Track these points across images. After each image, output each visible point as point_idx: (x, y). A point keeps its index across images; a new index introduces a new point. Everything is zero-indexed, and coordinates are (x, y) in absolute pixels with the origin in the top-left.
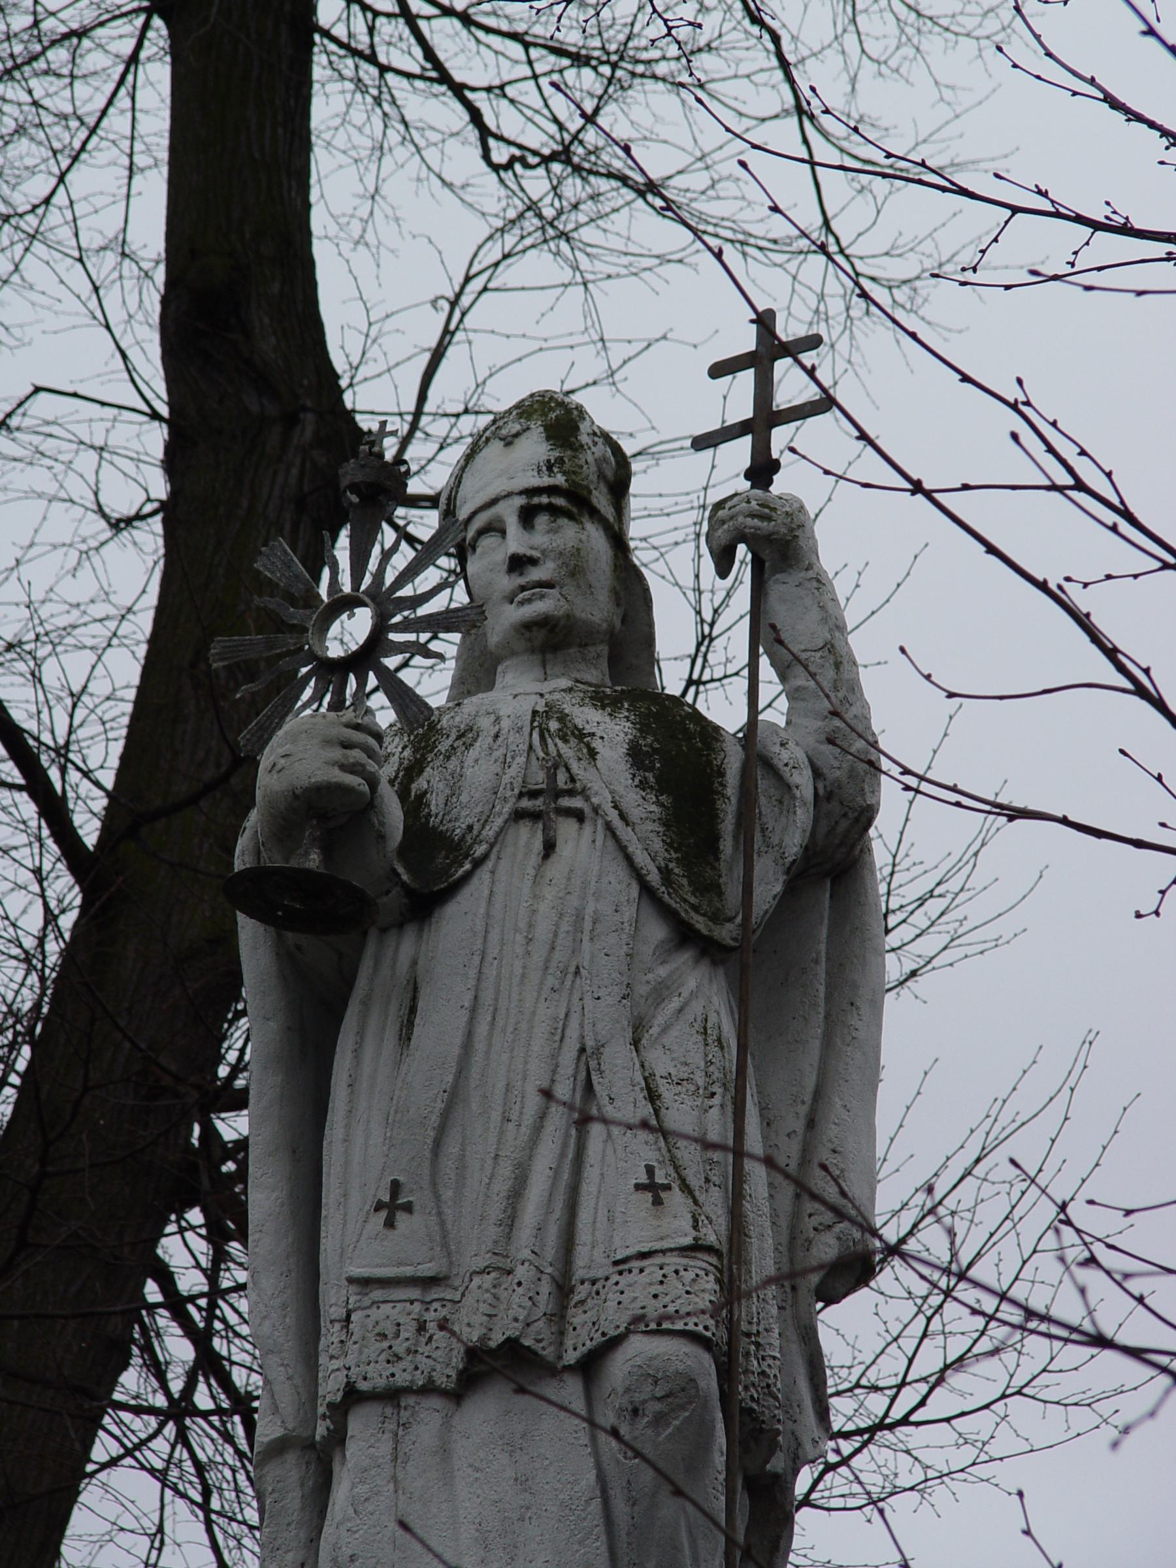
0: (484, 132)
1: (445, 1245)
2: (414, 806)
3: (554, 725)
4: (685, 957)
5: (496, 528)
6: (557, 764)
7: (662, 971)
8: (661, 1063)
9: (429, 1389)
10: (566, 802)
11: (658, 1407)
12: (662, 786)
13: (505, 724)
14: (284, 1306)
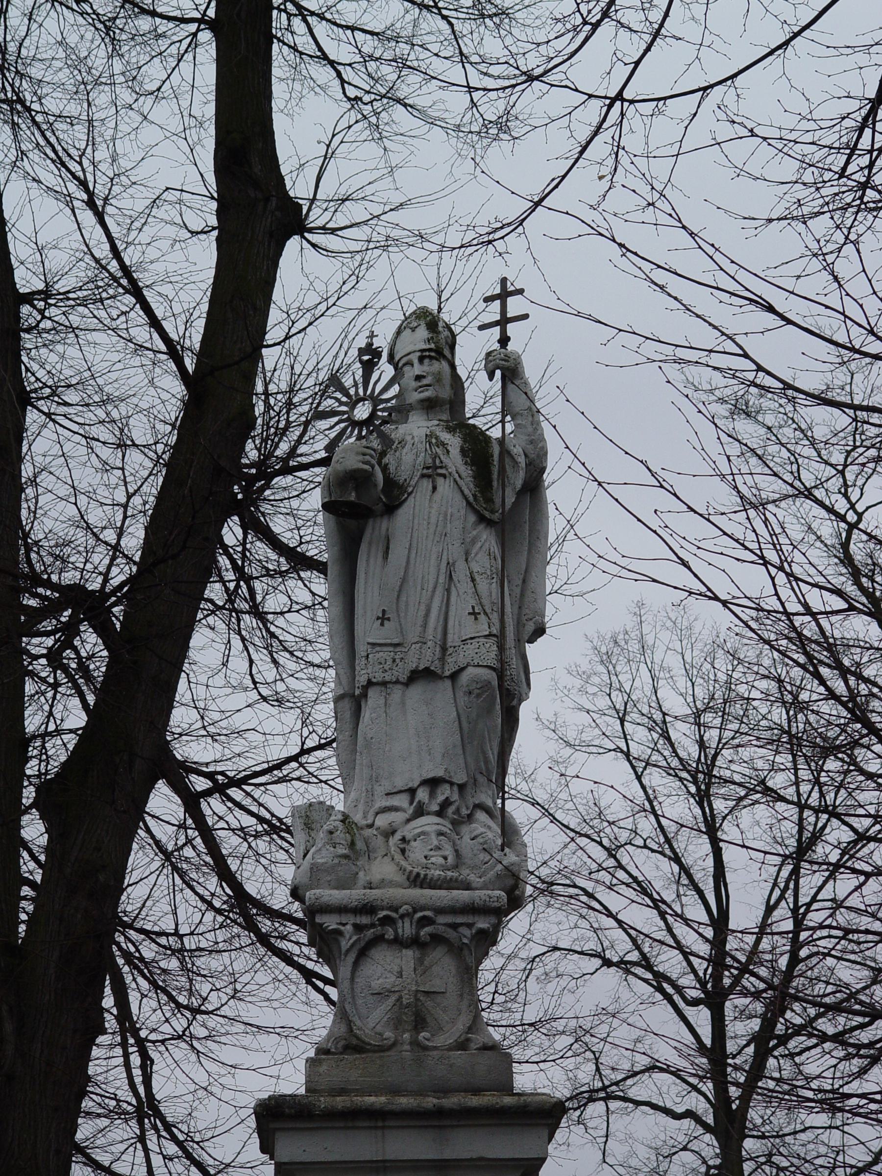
0: (343, 81)
1: (402, 632)
2: (385, 469)
3: (434, 441)
4: (482, 527)
5: (410, 363)
6: (436, 456)
7: (475, 533)
8: (476, 568)
9: (397, 682)
10: (440, 471)
11: (478, 691)
12: (473, 464)
13: (416, 439)
14: (342, 648)
